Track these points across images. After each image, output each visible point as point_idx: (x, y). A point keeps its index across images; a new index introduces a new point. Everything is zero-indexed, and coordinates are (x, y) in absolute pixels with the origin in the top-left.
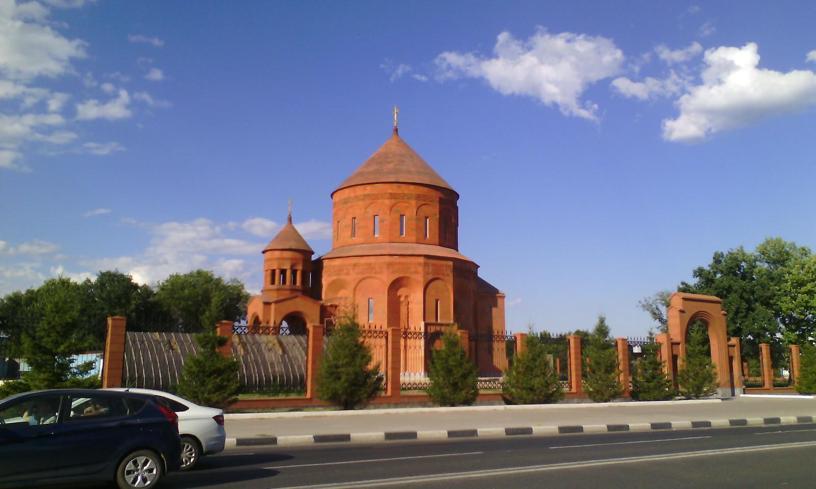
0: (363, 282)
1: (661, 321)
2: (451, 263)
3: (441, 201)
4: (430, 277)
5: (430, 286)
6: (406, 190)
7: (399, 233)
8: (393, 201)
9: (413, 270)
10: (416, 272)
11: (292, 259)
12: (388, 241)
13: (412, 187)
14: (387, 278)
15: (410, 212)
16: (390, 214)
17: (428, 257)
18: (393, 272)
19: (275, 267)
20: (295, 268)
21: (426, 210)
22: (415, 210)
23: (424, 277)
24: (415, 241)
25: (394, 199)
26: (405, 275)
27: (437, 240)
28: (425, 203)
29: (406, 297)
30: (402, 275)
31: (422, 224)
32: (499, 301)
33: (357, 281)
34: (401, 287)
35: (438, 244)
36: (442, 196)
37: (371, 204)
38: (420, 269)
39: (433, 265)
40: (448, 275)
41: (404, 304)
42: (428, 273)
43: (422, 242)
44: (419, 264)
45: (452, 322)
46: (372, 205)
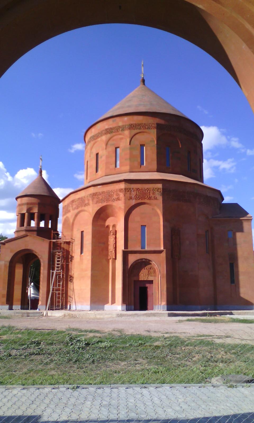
0: (78, 216)
1: (80, 330)
2: (160, 186)
3: (159, 127)
4: (133, 202)
5: (134, 212)
6: (120, 122)
7: (114, 165)
8: (109, 136)
9: (115, 197)
10: (118, 199)
11: (28, 204)
12: (104, 175)
13: (126, 118)
14: (91, 210)
15: (124, 140)
16: (106, 149)
17: (126, 181)
18: (97, 202)
19: (24, 211)
20: (31, 211)
21: (142, 138)
22: (128, 140)
23: (125, 203)
24: (128, 171)
25: (110, 133)
26: (108, 204)
27: (155, 166)
28: (138, 131)
29: (114, 226)
30: (104, 204)
31: (137, 152)
32: (245, 225)
33: (74, 216)
34: (108, 217)
35: (156, 170)
36: (162, 122)
37: (94, 144)
38: (122, 195)
39: (137, 189)
40: (156, 199)
41: (112, 234)
42: (131, 198)
43: (137, 170)
44: (121, 190)
45: (162, 248)
46: (95, 145)
